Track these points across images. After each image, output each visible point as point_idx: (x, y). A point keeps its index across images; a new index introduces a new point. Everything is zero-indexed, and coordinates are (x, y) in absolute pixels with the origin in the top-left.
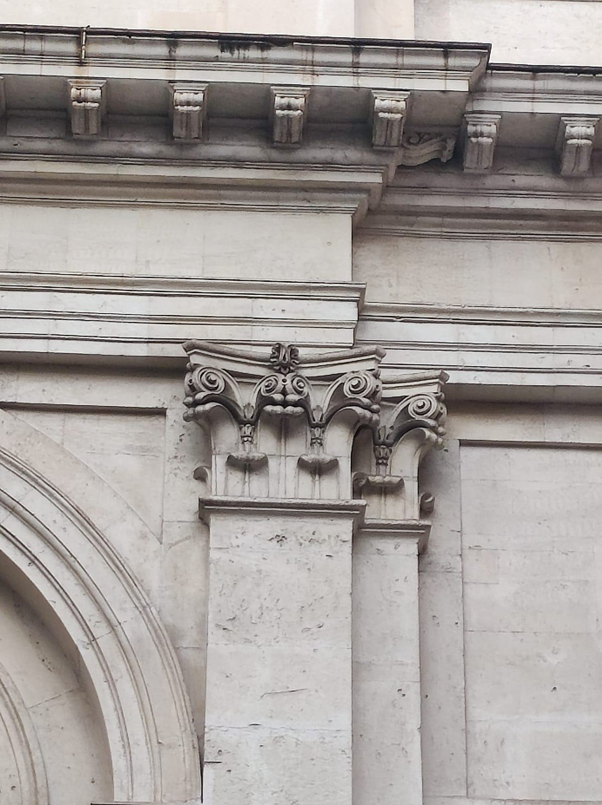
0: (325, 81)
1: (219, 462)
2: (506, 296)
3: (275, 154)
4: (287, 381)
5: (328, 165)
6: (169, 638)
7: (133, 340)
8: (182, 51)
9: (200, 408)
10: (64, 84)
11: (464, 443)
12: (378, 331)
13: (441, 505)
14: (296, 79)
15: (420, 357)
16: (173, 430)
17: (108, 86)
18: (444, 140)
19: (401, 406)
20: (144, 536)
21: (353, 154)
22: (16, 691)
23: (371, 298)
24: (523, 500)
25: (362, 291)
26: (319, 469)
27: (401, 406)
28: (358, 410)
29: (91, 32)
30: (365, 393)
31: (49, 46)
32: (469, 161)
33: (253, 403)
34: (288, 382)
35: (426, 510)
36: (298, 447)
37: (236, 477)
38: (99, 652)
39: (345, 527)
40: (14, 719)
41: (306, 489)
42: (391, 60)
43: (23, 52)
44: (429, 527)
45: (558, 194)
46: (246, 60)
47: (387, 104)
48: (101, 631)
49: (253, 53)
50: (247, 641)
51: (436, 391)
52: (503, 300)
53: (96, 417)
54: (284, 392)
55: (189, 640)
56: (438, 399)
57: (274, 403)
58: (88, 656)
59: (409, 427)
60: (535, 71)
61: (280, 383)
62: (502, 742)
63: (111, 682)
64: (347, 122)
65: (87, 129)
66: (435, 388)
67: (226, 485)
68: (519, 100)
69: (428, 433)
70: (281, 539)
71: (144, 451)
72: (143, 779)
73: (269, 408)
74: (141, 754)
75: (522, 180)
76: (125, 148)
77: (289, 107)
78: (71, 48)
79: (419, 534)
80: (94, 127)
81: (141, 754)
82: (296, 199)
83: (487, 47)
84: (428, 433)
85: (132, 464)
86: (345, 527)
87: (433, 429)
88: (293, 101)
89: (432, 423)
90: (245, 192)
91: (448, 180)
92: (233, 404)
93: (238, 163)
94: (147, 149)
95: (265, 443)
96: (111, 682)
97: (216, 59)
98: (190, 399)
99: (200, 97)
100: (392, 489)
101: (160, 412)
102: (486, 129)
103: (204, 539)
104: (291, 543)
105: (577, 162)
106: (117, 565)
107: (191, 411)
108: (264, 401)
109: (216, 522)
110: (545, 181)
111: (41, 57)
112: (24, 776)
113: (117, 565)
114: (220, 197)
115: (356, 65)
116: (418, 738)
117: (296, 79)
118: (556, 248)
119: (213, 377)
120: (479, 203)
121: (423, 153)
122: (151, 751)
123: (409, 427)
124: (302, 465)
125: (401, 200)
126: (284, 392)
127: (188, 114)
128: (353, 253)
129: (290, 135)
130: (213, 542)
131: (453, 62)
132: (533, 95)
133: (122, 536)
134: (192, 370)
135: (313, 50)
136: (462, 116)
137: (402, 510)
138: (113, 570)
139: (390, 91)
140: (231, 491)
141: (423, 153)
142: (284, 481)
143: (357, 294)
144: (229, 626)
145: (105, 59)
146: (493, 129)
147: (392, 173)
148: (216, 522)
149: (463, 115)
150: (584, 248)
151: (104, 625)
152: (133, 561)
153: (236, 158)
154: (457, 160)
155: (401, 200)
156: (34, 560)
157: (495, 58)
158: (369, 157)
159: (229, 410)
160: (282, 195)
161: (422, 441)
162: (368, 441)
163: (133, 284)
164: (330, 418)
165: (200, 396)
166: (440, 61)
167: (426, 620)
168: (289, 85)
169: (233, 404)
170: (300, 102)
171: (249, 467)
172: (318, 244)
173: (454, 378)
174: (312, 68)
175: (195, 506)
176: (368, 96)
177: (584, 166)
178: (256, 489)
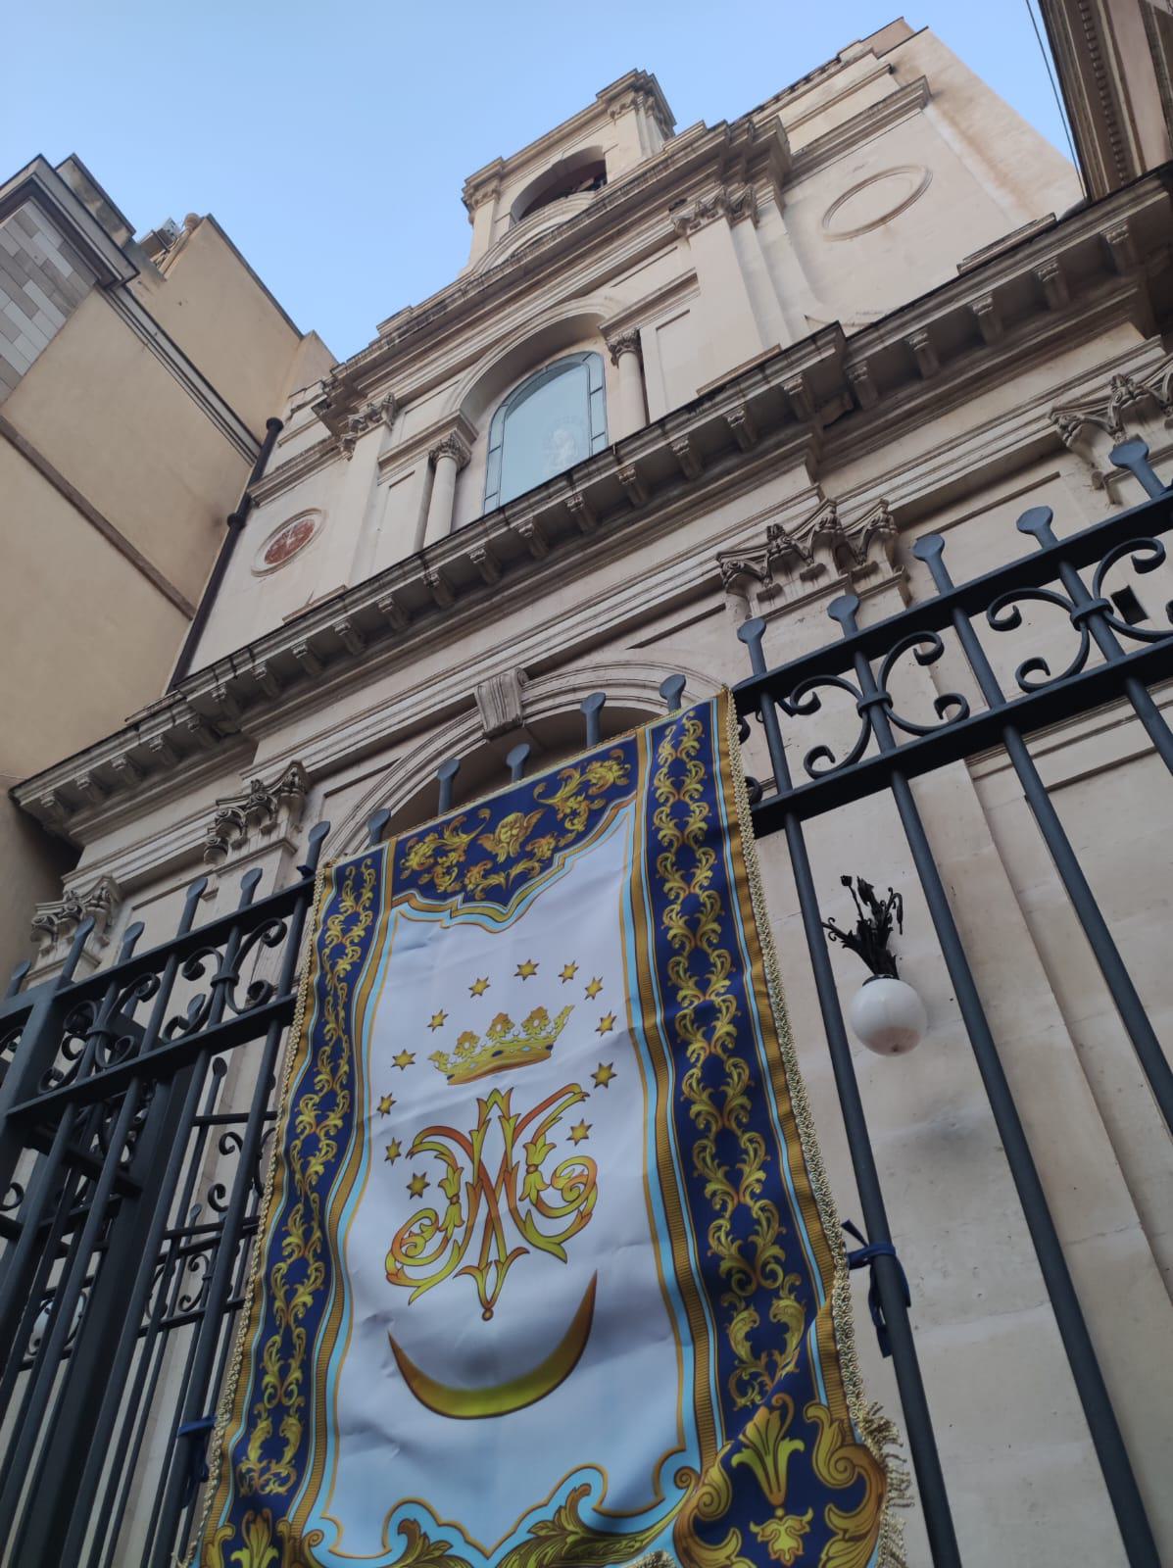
3: (746, 456)
8: (669, 426)
46: (704, 411)
47: (791, 384)
49: (707, 405)
70: (801, 620)
75: (901, 395)
77: (737, 419)
90: (669, 394)
97: (688, 420)
101: (722, 608)
111: (599, 471)
114: (728, 495)
121: (833, 411)
132: (881, 338)
135: (739, 384)
147: (820, 431)
154: (857, 407)
157: (848, 332)
160: (760, 475)
176: (779, 387)
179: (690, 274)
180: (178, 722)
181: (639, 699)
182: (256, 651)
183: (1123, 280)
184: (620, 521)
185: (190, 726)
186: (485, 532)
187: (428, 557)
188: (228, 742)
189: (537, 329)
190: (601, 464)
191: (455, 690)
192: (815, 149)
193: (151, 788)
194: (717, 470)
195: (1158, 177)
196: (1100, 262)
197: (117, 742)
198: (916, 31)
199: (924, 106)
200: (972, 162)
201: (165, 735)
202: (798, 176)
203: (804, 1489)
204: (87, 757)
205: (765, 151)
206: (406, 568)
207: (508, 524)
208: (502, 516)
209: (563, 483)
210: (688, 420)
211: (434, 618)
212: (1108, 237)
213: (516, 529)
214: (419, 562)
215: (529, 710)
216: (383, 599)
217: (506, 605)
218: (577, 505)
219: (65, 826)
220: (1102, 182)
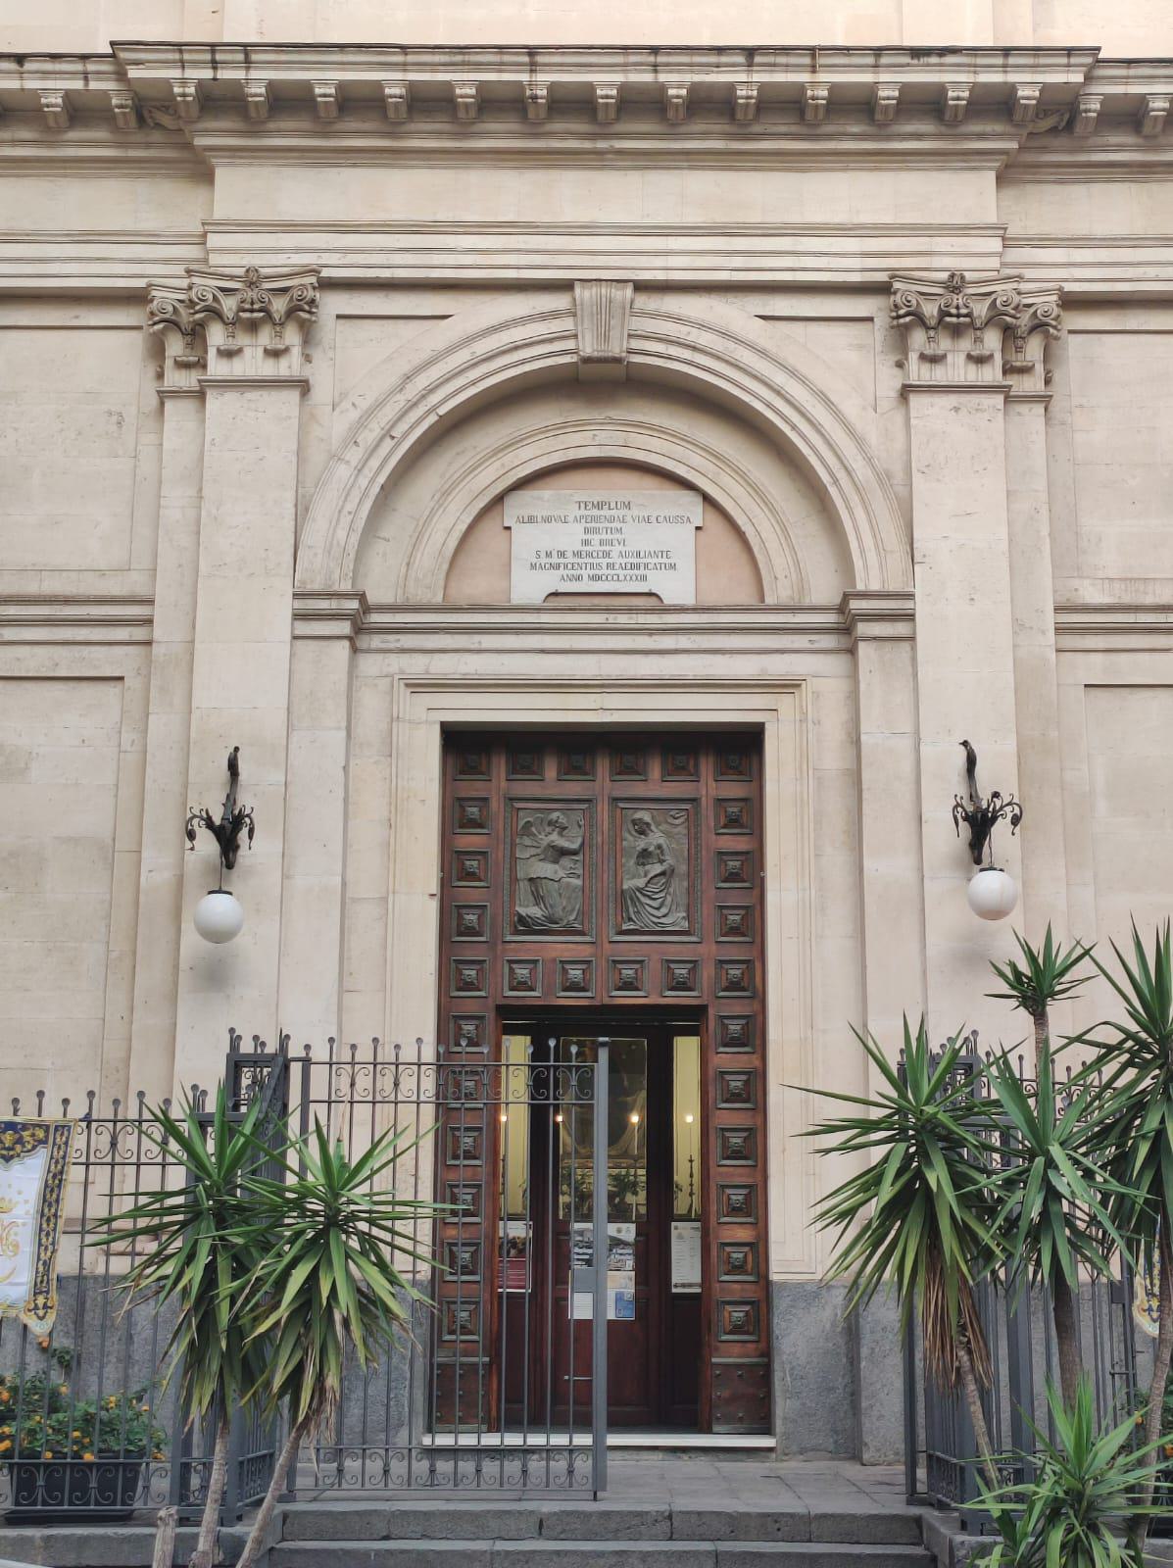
0: (985, 78)
1: (913, 357)
2: (1105, 224)
3: (943, 129)
4: (959, 300)
5: (981, 136)
6: (884, 478)
8: (884, 60)
9: (902, 321)
12: (1015, 255)
13: (1057, 376)
16: (879, 331)
18: (1062, 115)
19: (1032, 310)
20: (864, 408)
21: (998, 128)
22: (784, 513)
23: (1011, 232)
24: (1118, 376)
26: (980, 360)
27: (1032, 310)
28: (1008, 319)
30: (1012, 306)
31: (793, 60)
32: (1079, 129)
33: (935, 313)
34: (960, 301)
35: (1047, 382)
36: (966, 344)
37: (926, 367)
41: (972, 375)
43: (775, 65)
44: (1051, 396)
45: (1138, 148)
46: (928, 65)
48: (841, 475)
49: (934, 60)
50: (938, 480)
52: (1100, 230)
53: (826, 323)
54: (957, 308)
56: (1058, 305)
57: (951, 315)
58: (833, 491)
59: (1039, 326)
61: (955, 301)
62: (1100, 540)
64: (997, 104)
65: (816, 116)
66: (1055, 298)
67: (919, 373)
68: (1116, 84)
69: (1051, 330)
70: (956, 409)
72: (874, 572)
73: (948, 319)
74: (872, 556)
75: (1114, 139)
76: (841, 129)
77: (958, 98)
79: (1045, 400)
80: (821, 115)
81: (872, 556)
82: (958, 161)
83: (1098, 49)
84: (1051, 330)
86: (999, 399)
87: (1055, 327)
88: (962, 94)
89: (1054, 323)
92: (923, 317)
93: (918, 136)
94: (855, 129)
95: (944, 343)
97: (908, 65)
98: (894, 314)
99: (896, 94)
101: (870, 319)
102: (1093, 107)
103: (903, 412)
104: (964, 411)
105: (1154, 127)
106: (850, 431)
107: (895, 322)
108: (944, 313)
110: (1130, 139)
112: (792, 570)
113: (850, 431)
115: (1005, 66)
116: (1048, 540)
119: (909, 298)
121: (1046, 124)
122: (879, 554)
123: (1039, 326)
124: (970, 357)
126: (957, 308)
127: (887, 106)
128: (997, 198)
129: (956, 116)
130: (913, 414)
131: (1073, 60)
133: (851, 408)
134: (895, 293)
135: (976, 55)
136: (1077, 97)
137: (1033, 384)
139: (1028, 84)
140: (922, 377)
141: (1046, 124)
144: (925, 470)
146: (1098, 106)
147: (1024, 138)
149: (1077, 96)
150: (1154, 187)
151: (843, 471)
152: (859, 425)
153: (919, 136)
154: (1070, 126)
155: (1030, 158)
156: (794, 427)
157: (1101, 56)
158: (1009, 129)
159: (920, 319)
161: (1047, 335)
162: (1009, 333)
163: (850, 229)
165: (902, 312)
166: (1064, 60)
167: (1051, 456)
169: (923, 317)
170: (966, 94)
171: (935, 360)
173: (1068, 287)
174: (975, 68)
175: (899, 386)
176: (1012, 88)
177: (1159, 127)
178: (939, 375)
181: (769, 405)
184: (783, 129)
186: (624, 67)
187: (540, 59)
188: (157, 136)
191: (538, 259)
194: (909, 128)
206: (507, 58)
210: (908, 65)
215: (636, 344)
216: (464, 83)
217: (610, 156)
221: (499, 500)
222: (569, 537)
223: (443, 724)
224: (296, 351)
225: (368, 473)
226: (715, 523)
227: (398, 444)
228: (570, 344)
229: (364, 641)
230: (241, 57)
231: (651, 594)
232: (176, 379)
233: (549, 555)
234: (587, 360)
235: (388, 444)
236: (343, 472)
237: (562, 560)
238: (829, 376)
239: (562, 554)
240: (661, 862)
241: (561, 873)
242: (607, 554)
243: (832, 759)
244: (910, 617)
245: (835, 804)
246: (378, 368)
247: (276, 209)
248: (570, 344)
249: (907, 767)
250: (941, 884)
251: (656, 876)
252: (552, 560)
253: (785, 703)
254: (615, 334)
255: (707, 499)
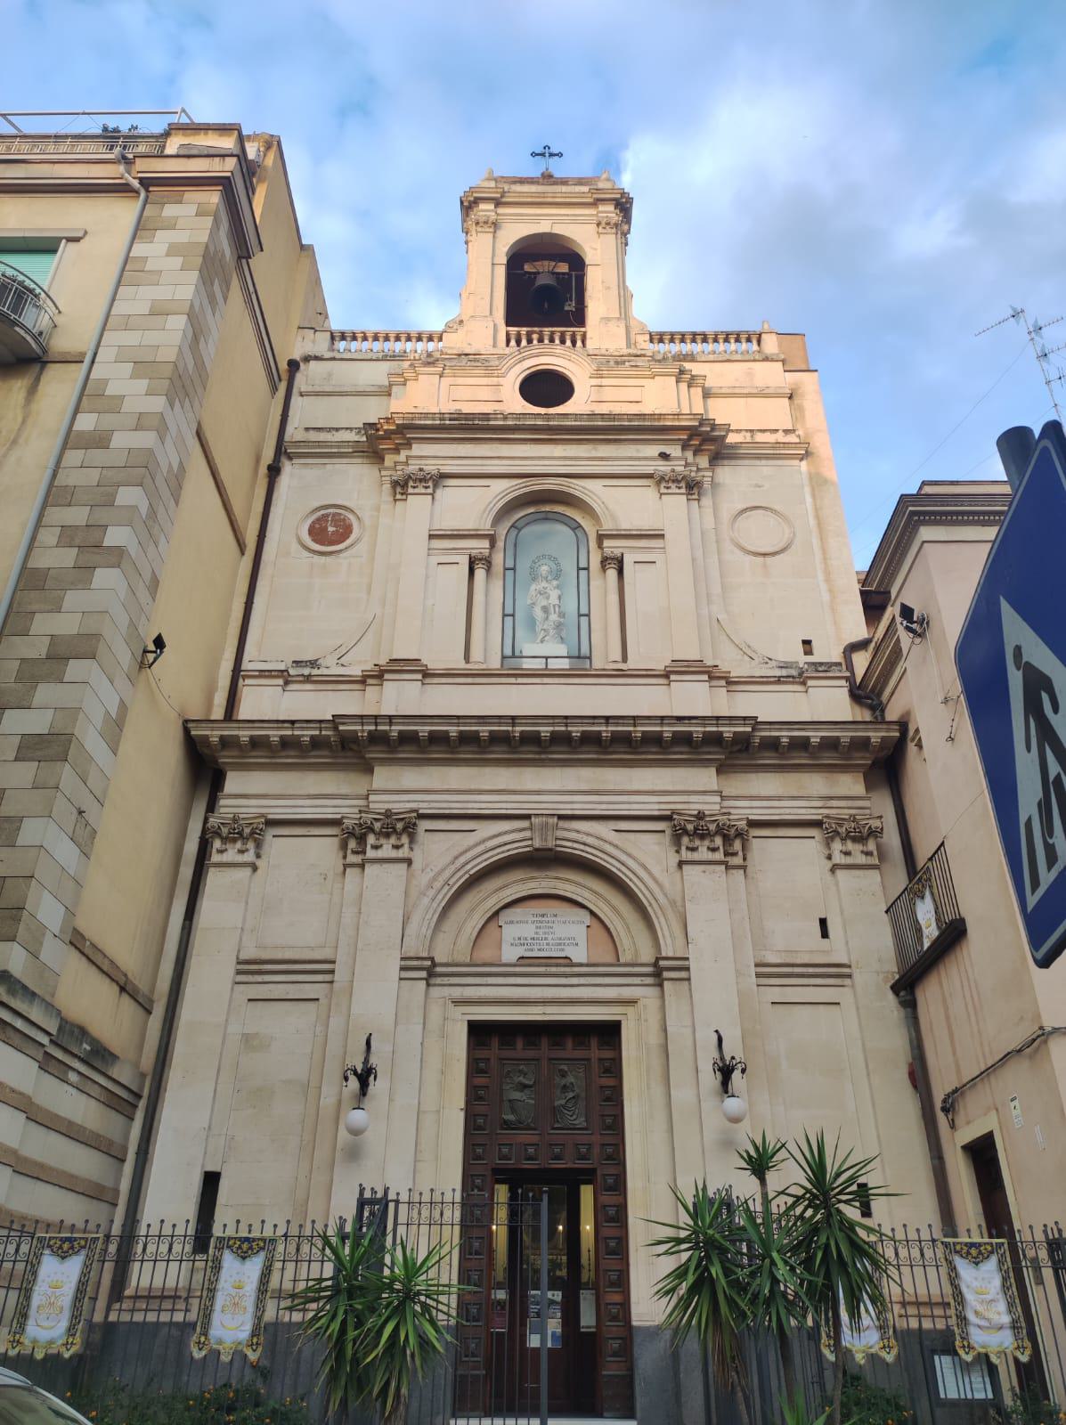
0: (708, 729)
1: (683, 848)
5: (709, 753)
7: (654, 810)
10: (630, 732)
11: (754, 837)
13: (748, 856)
14: (699, 729)
15: (743, 811)
17: (643, 732)
21: (716, 749)
25: (722, 792)
26: (714, 850)
29: (638, 717)
35: (745, 859)
36: (707, 843)
38: (652, 908)
39: (723, 867)
40: (594, 723)
42: (727, 722)
48: (653, 902)
49: (687, 722)
51: (995, 1111)
55: (679, 903)
59: (739, 834)
60: (770, 723)
63: (658, 918)
64: (715, 740)
67: (686, 855)
71: (659, 844)
72: (670, 948)
75: (767, 754)
78: (632, 722)
81: (669, 941)
85: (657, 848)
91: (474, 552)
92: (687, 831)
93: (682, 753)
94: (654, 750)
95: (697, 843)
96: (658, 918)
100: (735, 854)
101: (664, 831)
104: (707, 873)
109: (685, 867)
117: (699, 729)
118: (777, 774)
120: (754, 762)
124: (708, 848)
125: (729, 762)
132: (770, 730)
133: (656, 871)
137: (737, 860)
138: (662, 911)
139: (728, 731)
142: (703, 854)
143: (720, 793)
145: (642, 725)
148: (685, 867)
154: (747, 749)
155: (729, 762)
157: (758, 720)
162: (727, 840)
164: (716, 833)
166: (742, 722)
168: (697, 730)
169: (687, 831)
171: (693, 849)
172: (705, 778)
176: (721, 733)
178: (695, 856)
179: (660, 532)
180: (323, 733)
182: (394, 721)
183: (868, 755)
185: (332, 739)
188: (349, 754)
189: (552, 487)
190: (625, 722)
192: (739, 448)
193: (287, 757)
194: (677, 749)
195: (900, 726)
196: (862, 744)
197: (276, 725)
198: (811, 369)
199: (801, 460)
200: (815, 542)
201: (312, 737)
202: (723, 458)
203: (889, 1347)
204: (250, 725)
205: (714, 440)
207: (567, 726)
208: (565, 721)
209: (603, 721)
211: (505, 749)
212: (872, 740)
213: (570, 732)
214: (511, 721)
215: (559, 842)
216: (483, 731)
218: (607, 737)
219: (217, 755)
220: (875, 672)
221: (496, 914)
222: (528, 930)
223: (468, 1021)
224: (406, 846)
225: (437, 901)
226: (596, 924)
227: (451, 888)
228: (529, 843)
229: (433, 981)
230: (388, 721)
231: (566, 958)
232: (352, 858)
233: (519, 939)
234: (537, 850)
235: (447, 887)
236: (426, 901)
237: (526, 942)
238: (646, 858)
239: (526, 939)
240: (573, 1091)
241: (524, 1098)
242: (546, 939)
243: (654, 1038)
244: (687, 969)
245: (656, 1062)
246: (442, 854)
247: (401, 786)
248: (529, 843)
249: (690, 1043)
250: (710, 1103)
251: (570, 1099)
252: (520, 942)
253: (630, 1010)
254: (549, 838)
255: (592, 913)
